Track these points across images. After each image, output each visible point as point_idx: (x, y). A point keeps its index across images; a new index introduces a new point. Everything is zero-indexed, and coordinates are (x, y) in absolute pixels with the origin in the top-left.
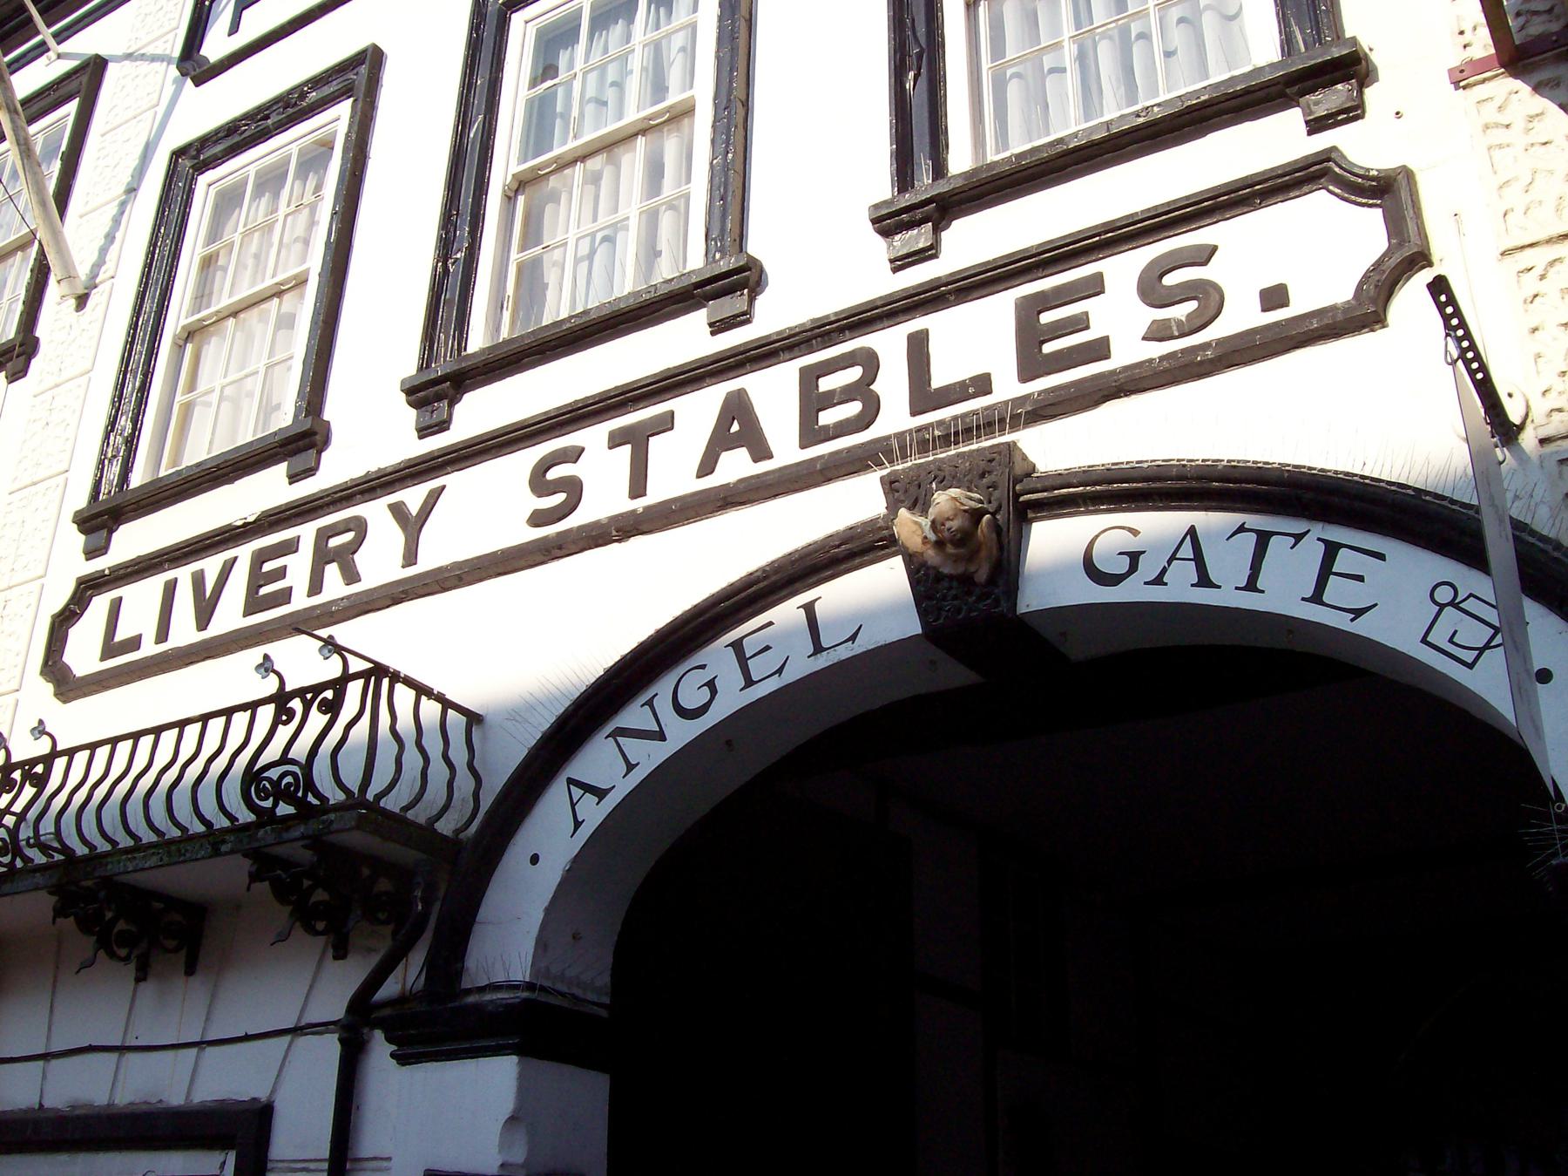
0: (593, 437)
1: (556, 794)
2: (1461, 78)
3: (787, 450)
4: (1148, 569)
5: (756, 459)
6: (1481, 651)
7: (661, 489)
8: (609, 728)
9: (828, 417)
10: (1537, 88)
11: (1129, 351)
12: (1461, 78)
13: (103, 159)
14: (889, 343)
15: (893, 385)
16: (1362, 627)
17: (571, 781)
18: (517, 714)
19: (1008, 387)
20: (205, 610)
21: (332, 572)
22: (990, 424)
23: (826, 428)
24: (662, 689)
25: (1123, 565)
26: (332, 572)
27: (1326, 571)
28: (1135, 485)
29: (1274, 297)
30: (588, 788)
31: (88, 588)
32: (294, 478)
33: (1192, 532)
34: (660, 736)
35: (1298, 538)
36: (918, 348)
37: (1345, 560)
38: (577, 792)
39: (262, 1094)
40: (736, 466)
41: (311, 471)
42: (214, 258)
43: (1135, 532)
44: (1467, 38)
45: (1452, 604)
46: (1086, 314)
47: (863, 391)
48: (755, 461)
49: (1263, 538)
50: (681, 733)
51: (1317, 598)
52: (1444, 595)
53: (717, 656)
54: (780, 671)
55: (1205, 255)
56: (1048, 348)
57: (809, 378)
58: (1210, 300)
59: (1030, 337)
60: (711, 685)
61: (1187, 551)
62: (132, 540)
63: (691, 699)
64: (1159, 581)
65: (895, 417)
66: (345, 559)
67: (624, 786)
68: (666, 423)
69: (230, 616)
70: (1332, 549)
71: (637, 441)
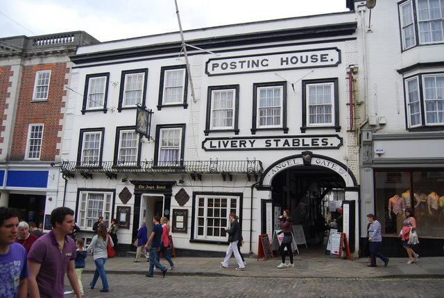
0: (272, 140)
3: (291, 146)
5: (285, 133)
7: (279, 146)
11: (320, 146)
14: (301, 139)
15: (301, 143)
19: (311, 146)
20: (225, 146)
29: (332, 145)
31: (207, 139)
36: (303, 140)
40: (286, 146)
42: (403, 203)
50: (283, 168)
58: (327, 143)
59: (313, 142)
62: (211, 135)
65: (301, 146)
68: (280, 140)
71: (277, 141)
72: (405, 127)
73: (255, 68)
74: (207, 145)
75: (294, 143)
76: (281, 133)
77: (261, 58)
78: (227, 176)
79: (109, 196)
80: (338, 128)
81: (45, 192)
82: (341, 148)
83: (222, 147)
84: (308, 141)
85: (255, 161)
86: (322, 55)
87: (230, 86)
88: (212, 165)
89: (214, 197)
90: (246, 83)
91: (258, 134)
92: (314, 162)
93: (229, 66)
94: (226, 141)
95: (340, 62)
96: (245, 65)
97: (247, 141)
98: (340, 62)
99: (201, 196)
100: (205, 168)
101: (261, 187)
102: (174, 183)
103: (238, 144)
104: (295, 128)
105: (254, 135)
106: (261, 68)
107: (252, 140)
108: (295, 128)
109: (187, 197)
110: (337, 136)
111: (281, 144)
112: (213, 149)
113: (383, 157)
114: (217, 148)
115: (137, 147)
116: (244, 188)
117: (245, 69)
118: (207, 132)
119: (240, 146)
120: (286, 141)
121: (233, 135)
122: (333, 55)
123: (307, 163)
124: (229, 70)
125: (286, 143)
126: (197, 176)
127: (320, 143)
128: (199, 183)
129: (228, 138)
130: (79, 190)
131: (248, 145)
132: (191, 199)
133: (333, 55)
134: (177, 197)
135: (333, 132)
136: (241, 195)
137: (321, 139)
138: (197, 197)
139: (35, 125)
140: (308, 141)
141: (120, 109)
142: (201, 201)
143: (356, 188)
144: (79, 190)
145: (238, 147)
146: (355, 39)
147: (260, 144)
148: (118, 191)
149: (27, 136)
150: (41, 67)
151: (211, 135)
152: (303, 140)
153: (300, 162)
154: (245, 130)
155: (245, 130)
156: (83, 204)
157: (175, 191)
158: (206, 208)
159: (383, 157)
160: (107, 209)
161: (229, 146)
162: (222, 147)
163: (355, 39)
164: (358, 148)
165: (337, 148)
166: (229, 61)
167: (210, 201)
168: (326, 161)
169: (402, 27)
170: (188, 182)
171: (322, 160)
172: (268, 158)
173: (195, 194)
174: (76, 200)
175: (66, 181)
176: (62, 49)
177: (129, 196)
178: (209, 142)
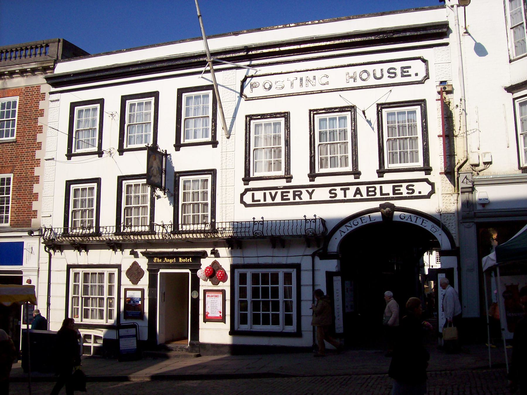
1: (338, 232)
2: (441, 173)
3: (365, 196)
4: (406, 218)
6: (435, 232)
7: (348, 197)
8: (345, 225)
9: (370, 193)
10: (447, 177)
11: (405, 194)
12: (441, 173)
13: (229, 110)
14: (378, 186)
15: (378, 191)
16: (425, 228)
17: (340, 230)
18: (332, 220)
19: (391, 195)
20: (273, 198)
21: (297, 197)
22: (389, 199)
23: (370, 195)
24: (352, 222)
25: (403, 218)
26: (297, 197)
27: (423, 222)
28: (29, 339)
29: (420, 193)
30: (342, 232)
32: (355, 178)
33: (410, 216)
34: (351, 227)
35: (420, 218)
37: (424, 221)
38: (341, 232)
39: (299, 262)
40: (358, 197)
41: (248, 184)
43: (405, 215)
44: (442, 169)
45: (433, 227)
46: (23, 242)
47: (374, 191)
48: (367, 196)
49: (417, 218)
50: (354, 227)
51: (362, 223)
52: (433, 226)
53: (358, 219)
54: (366, 222)
55: (413, 186)
56: (396, 192)
57: (368, 188)
58: (413, 191)
60: (358, 222)
61: (410, 217)
62: (252, 184)
63: (356, 224)
64: (407, 220)
65: (378, 195)
66: (299, 196)
67: (347, 232)
68: (348, 189)
69: (278, 199)
70: (423, 220)
71: (345, 190)
74: (248, 198)
75: (294, 196)
76: (350, 179)
79: (288, 278)
80: (427, 170)
84: (388, 189)
91: (319, 181)
94: (273, 192)
95: (427, 77)
97: (304, 190)
98: (427, 77)
101: (325, 255)
102: (204, 255)
103: (291, 196)
107: (310, 190)
111: (350, 194)
112: (256, 204)
114: (262, 202)
118: (247, 179)
119: (294, 199)
120: (358, 189)
127: (404, 190)
130: (69, 267)
131: (305, 197)
132: (146, 275)
133: (417, 67)
135: (421, 175)
136: (298, 267)
137: (405, 185)
140: (388, 189)
141: (121, 151)
144: (69, 267)
145: (292, 200)
146: (447, 44)
147: (322, 194)
148: (125, 268)
152: (381, 188)
156: (76, 287)
158: (249, 286)
161: (278, 199)
167: (255, 277)
177: (141, 274)
178: (249, 194)
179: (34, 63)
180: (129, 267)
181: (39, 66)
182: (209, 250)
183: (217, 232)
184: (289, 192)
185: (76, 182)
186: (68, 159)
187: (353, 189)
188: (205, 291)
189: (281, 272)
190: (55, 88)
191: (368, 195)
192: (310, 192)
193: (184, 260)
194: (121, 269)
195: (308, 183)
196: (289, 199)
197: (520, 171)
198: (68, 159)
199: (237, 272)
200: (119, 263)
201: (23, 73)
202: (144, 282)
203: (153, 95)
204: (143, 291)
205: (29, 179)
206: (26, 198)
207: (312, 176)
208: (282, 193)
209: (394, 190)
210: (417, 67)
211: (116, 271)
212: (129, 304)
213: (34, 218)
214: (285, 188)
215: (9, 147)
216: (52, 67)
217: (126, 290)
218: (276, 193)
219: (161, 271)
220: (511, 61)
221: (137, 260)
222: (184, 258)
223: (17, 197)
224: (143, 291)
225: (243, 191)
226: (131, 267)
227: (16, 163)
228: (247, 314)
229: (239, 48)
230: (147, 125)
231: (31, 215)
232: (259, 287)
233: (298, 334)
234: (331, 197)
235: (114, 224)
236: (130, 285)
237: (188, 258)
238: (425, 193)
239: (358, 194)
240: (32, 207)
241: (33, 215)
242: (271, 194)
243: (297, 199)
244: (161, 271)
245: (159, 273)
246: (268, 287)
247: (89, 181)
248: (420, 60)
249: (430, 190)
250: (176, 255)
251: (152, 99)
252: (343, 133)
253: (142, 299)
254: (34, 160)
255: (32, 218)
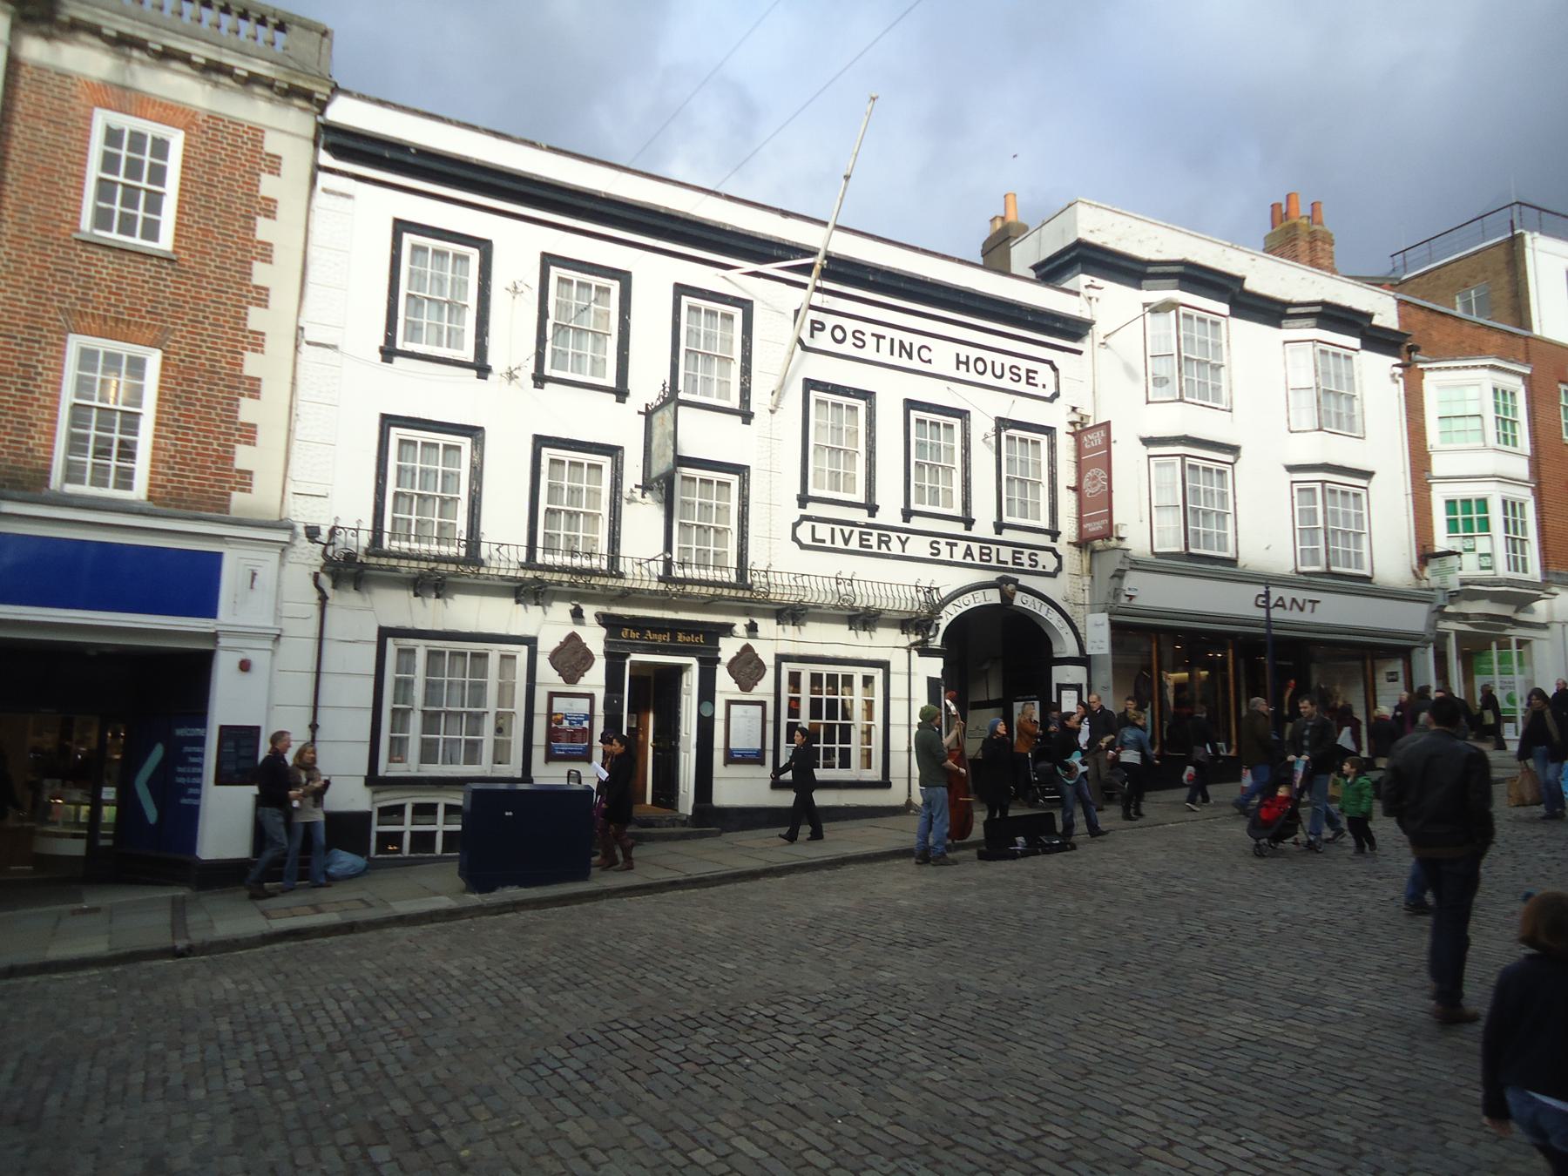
3: (977, 561)
12: (1069, 543)
14: (994, 547)
15: (994, 555)
19: (1010, 565)
20: (846, 541)
21: (883, 545)
26: (883, 545)
29: (1044, 567)
36: (998, 550)
40: (969, 560)
47: (989, 555)
50: (965, 608)
57: (981, 548)
62: (813, 509)
66: (887, 543)
67: (955, 615)
68: (956, 545)
71: (952, 545)
72: (1149, 548)
73: (904, 362)
74: (804, 532)
75: (880, 542)
76: (958, 529)
77: (918, 341)
78: (864, 619)
79: (868, 681)
80: (1054, 534)
81: (214, 637)
82: (1059, 574)
83: (839, 544)
84: (1006, 554)
85: (357, 530)
86: (1028, 371)
87: (855, 390)
88: (841, 588)
89: (825, 670)
90: (891, 391)
91: (917, 523)
92: (1020, 600)
93: (850, 339)
94: (847, 530)
95: (1056, 395)
96: (885, 344)
97: (893, 535)
98: (1056, 395)
99: (795, 666)
100: (818, 592)
101: (925, 651)
102: (727, 630)
103: (874, 541)
104: (984, 527)
105: (998, 537)
106: (915, 364)
107: (903, 536)
108: (984, 527)
109: (760, 668)
110: (1053, 550)
111: (958, 555)
112: (817, 546)
113: (1135, 602)
114: (828, 544)
115: (605, 510)
116: (887, 643)
117: (884, 357)
118: (804, 500)
119: (879, 548)
120: (969, 548)
121: (861, 516)
122: (1044, 373)
123: (1007, 598)
124: (847, 348)
125: (969, 552)
126: (793, 614)
127: (1025, 559)
128: (790, 630)
129: (854, 524)
130: (385, 633)
131: (896, 548)
132: (770, 674)
133: (1044, 374)
134: (732, 667)
135: (1045, 540)
136: (885, 665)
137: (1027, 552)
138: (786, 668)
139: (103, 345)
140: (1006, 554)
141: (540, 379)
142: (795, 679)
143: (1083, 660)
144: (385, 633)
145: (875, 549)
146: (1079, 353)
147: (920, 547)
148: (547, 644)
149: (57, 384)
150: (123, 97)
151: (813, 509)
153: (993, 597)
154: (890, 513)
155: (890, 513)
156: (404, 686)
157: (728, 648)
158: (805, 695)
159: (1135, 602)
160: (870, 716)
161: (854, 544)
162: (839, 544)
163: (1079, 353)
164: (1087, 580)
165: (1053, 575)
166: (851, 324)
167: (816, 679)
168: (1037, 600)
169: (1149, 354)
170: (766, 626)
171: (1031, 598)
172: (948, 580)
173: (781, 659)
174: (372, 670)
175: (323, 599)
176: (261, 68)
177: (587, 659)
178: (807, 525)
179: (268, 64)
180: (558, 644)
181: (284, 78)
182: (740, 623)
183: (481, 563)
184: (871, 534)
185: (451, 430)
186: (383, 360)
187: (962, 545)
188: (729, 703)
189: (858, 673)
190: (335, 158)
191: (981, 560)
192: (903, 539)
193: (688, 639)
194: (536, 648)
195: (901, 524)
196: (871, 547)
197: (1153, 557)
198: (383, 360)
199: (786, 668)
200: (530, 632)
201: (212, 70)
202: (595, 679)
203: (618, 275)
204: (591, 697)
205: (223, 380)
206: (212, 432)
207: (908, 514)
208: (861, 533)
209: (1014, 558)
210: (1044, 374)
211: (522, 652)
212: (559, 727)
213: (243, 490)
214: (868, 526)
215: (147, 269)
216: (324, 98)
217: (552, 695)
218: (852, 532)
219: (636, 657)
220: (1148, 402)
221: (579, 630)
222: (688, 633)
223: (178, 421)
224: (591, 697)
225: (797, 519)
226: (563, 645)
227: (176, 324)
228: (849, 749)
229: (639, 205)
230: (559, 331)
231: (229, 482)
232: (821, 699)
233: (885, 784)
234: (932, 554)
235: (524, 541)
236: (561, 685)
237: (697, 634)
238: (1050, 569)
239: (969, 555)
240: (233, 459)
241: (237, 483)
242: (842, 530)
243: (884, 550)
244: (636, 657)
245: (628, 661)
246: (821, 699)
247: (432, 427)
248: (1048, 366)
249: (1056, 565)
250: (675, 627)
251: (555, 272)
252: (935, 448)
253: (590, 717)
254: (243, 330)
255: (233, 489)
